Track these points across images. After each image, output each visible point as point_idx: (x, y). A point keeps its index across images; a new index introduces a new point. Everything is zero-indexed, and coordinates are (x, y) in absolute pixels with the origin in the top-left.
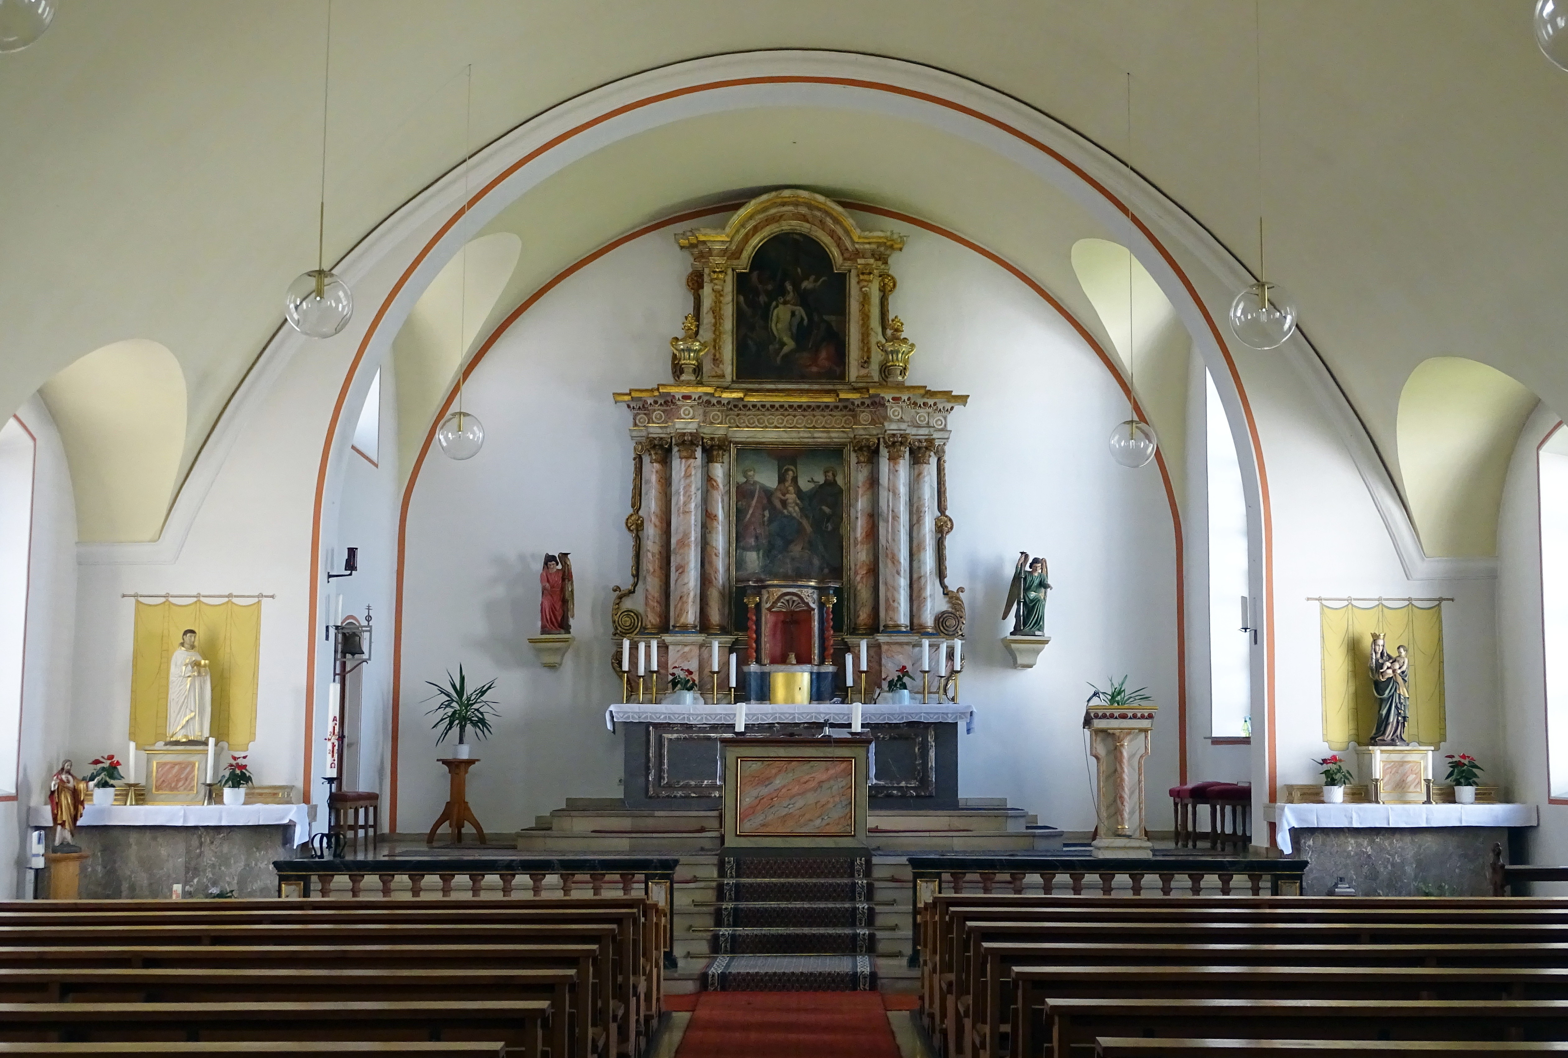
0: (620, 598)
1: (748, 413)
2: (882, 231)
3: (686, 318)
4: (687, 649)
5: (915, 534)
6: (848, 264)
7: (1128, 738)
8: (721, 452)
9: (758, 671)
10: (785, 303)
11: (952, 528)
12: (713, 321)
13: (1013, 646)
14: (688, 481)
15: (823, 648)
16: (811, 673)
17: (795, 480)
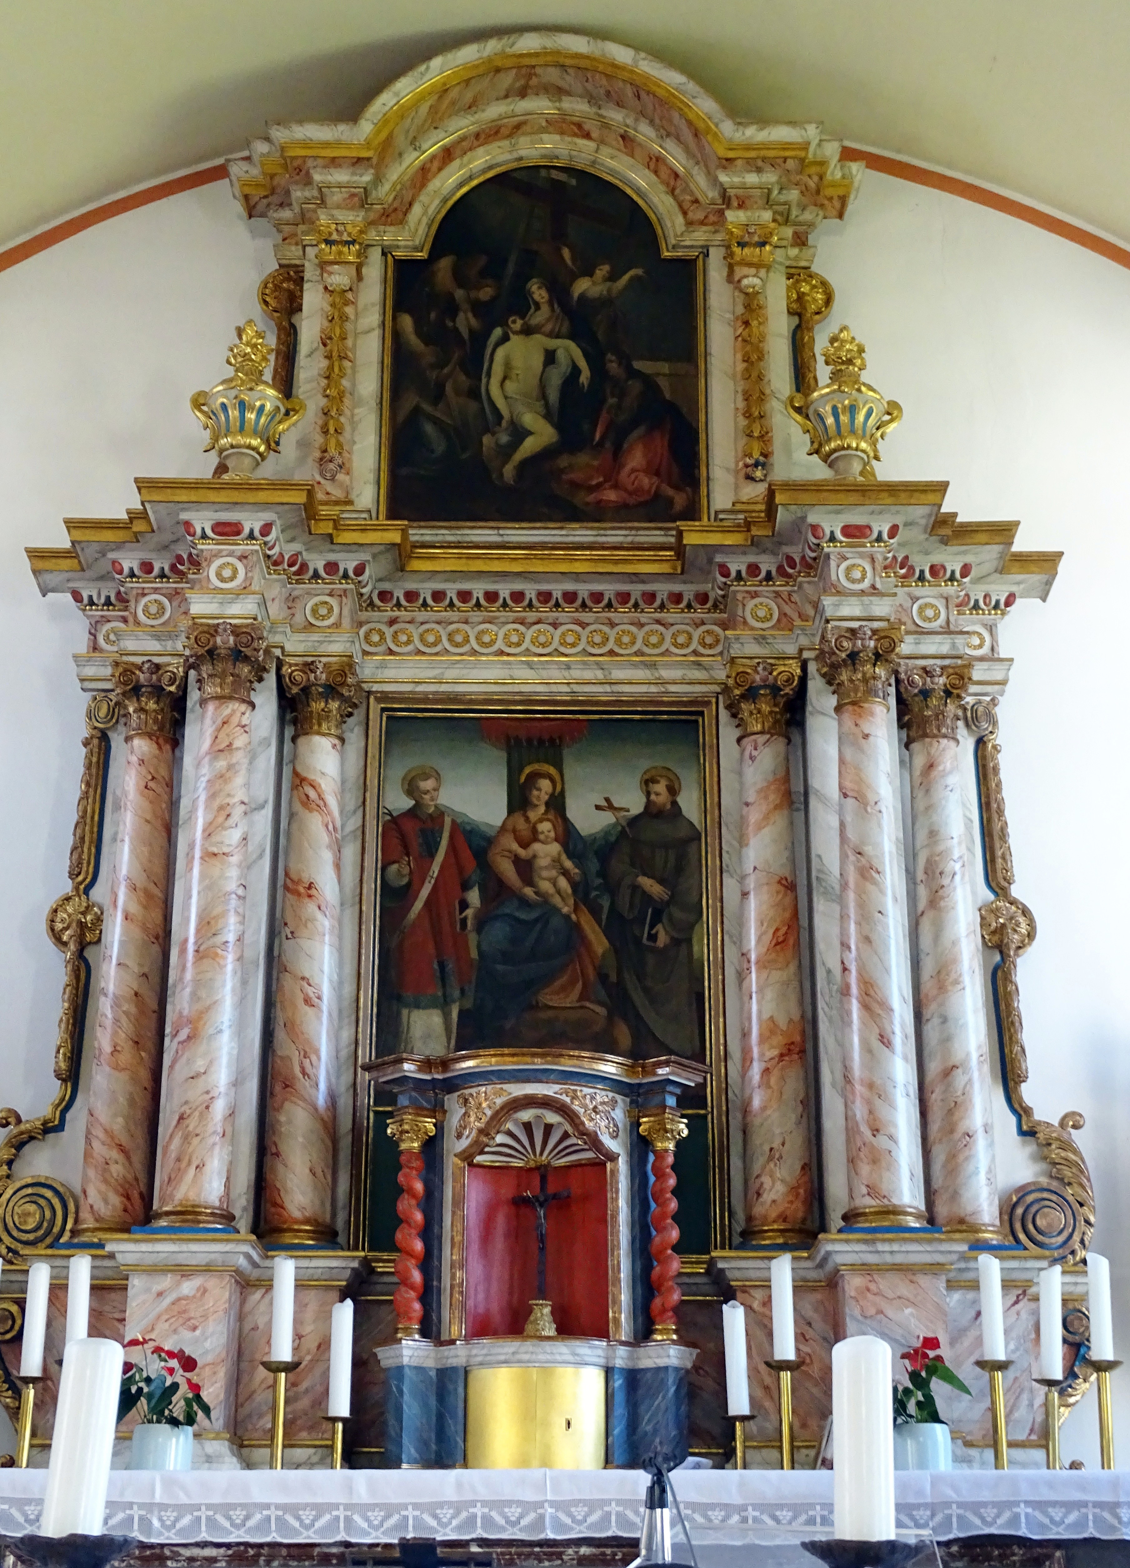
0: (19, 1144)
1: (422, 615)
2: (792, 123)
3: (240, 332)
4: (188, 1287)
5: (926, 941)
6: (700, 236)
8: (334, 705)
9: (430, 1363)
10: (527, 331)
11: (1031, 935)
12: (325, 363)
14: (221, 764)
15: (647, 1286)
16: (609, 1371)
17: (557, 804)
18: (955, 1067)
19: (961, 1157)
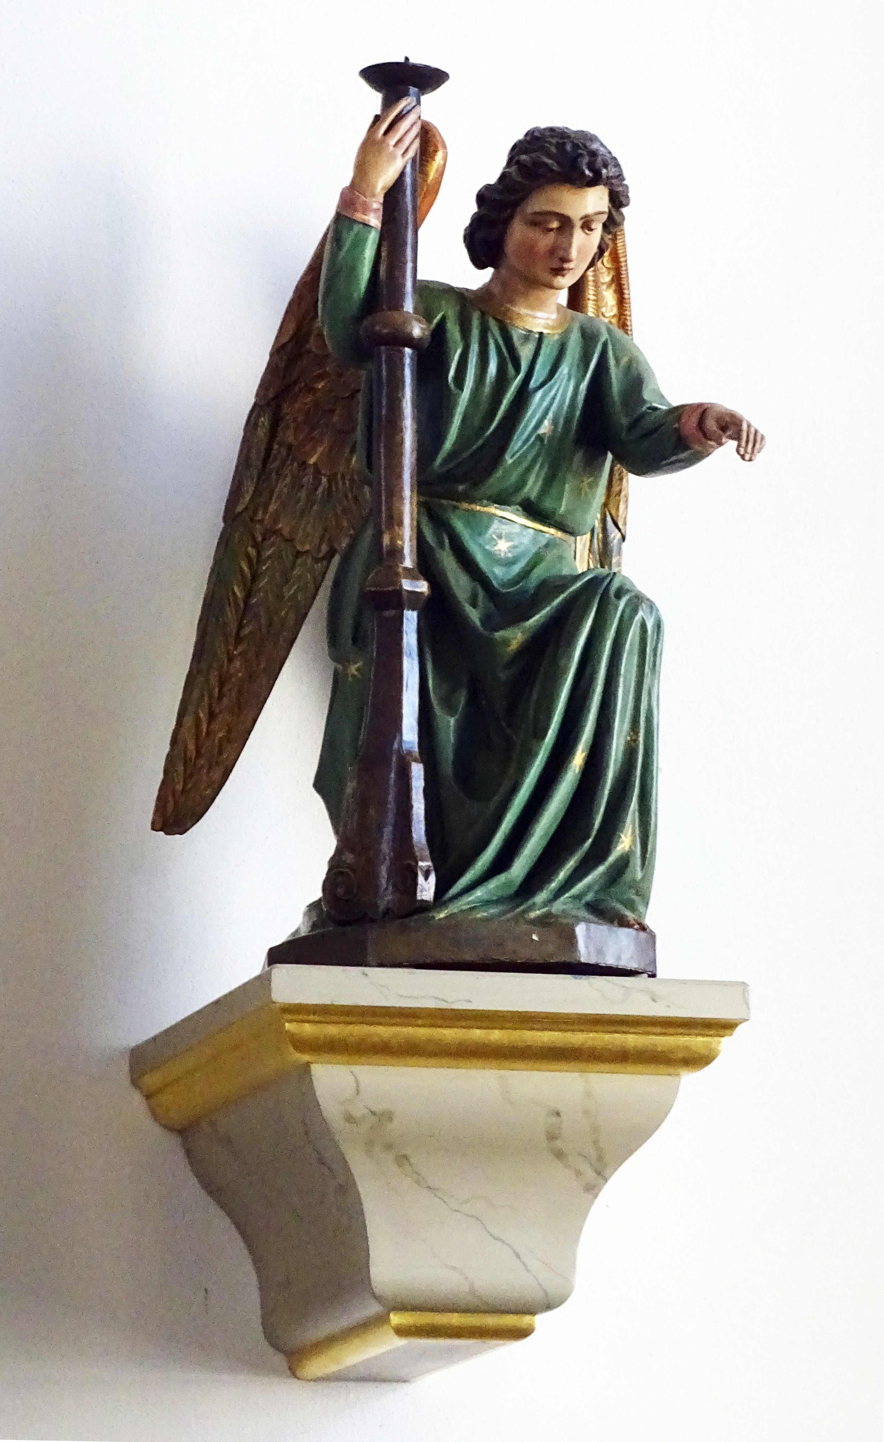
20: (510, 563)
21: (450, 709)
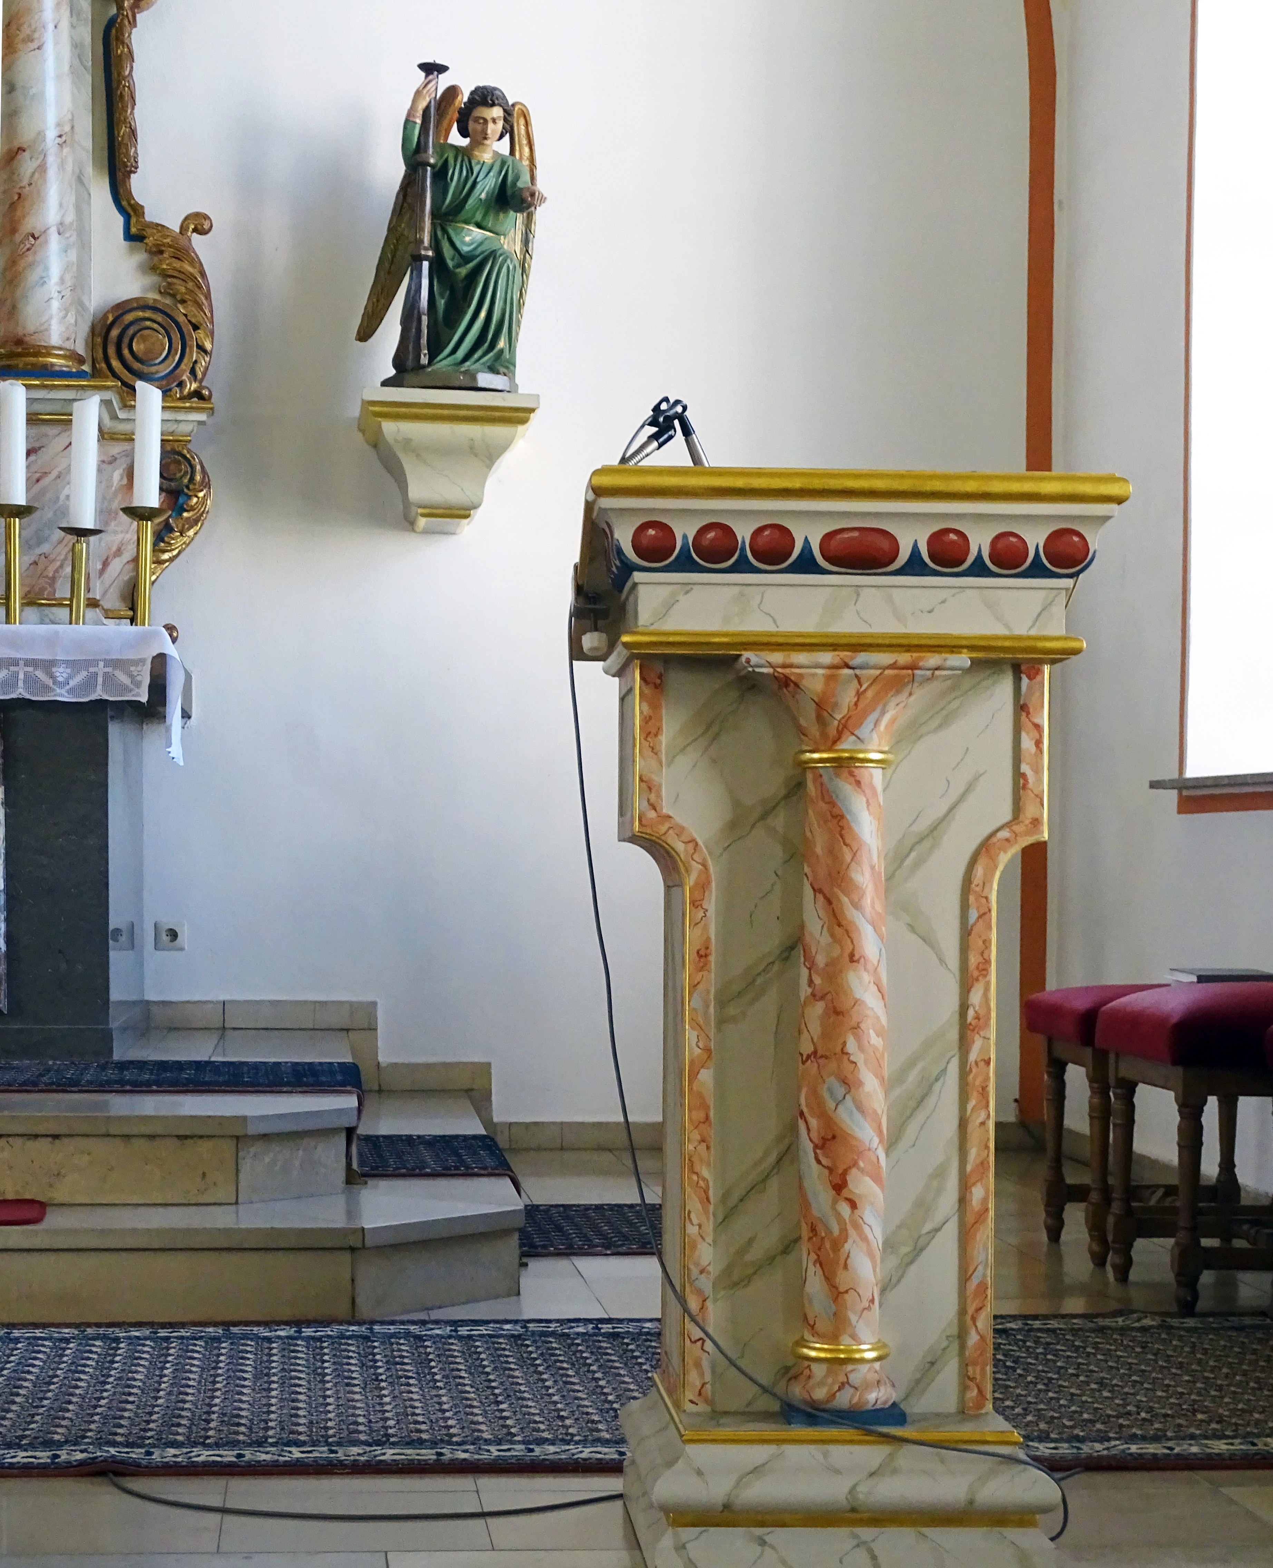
7: (895, 712)
13: (389, 428)
18: (21, 149)
19: (22, 263)
20: (469, 245)
21: (442, 297)
